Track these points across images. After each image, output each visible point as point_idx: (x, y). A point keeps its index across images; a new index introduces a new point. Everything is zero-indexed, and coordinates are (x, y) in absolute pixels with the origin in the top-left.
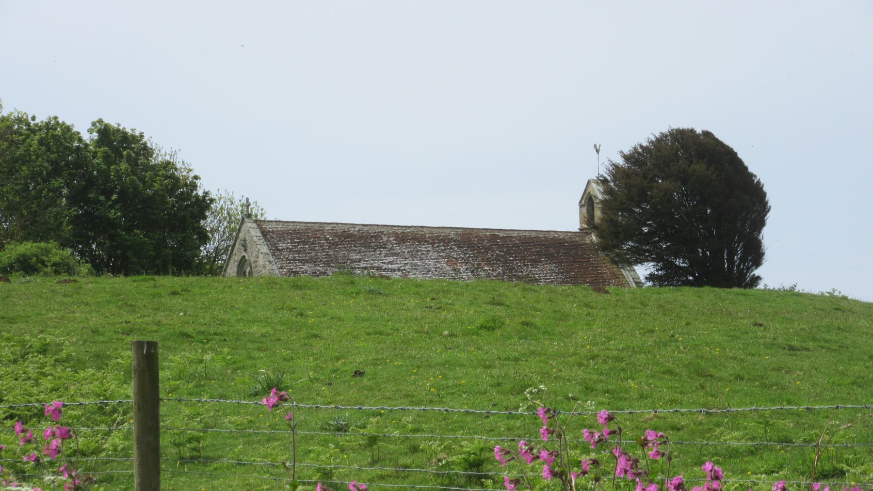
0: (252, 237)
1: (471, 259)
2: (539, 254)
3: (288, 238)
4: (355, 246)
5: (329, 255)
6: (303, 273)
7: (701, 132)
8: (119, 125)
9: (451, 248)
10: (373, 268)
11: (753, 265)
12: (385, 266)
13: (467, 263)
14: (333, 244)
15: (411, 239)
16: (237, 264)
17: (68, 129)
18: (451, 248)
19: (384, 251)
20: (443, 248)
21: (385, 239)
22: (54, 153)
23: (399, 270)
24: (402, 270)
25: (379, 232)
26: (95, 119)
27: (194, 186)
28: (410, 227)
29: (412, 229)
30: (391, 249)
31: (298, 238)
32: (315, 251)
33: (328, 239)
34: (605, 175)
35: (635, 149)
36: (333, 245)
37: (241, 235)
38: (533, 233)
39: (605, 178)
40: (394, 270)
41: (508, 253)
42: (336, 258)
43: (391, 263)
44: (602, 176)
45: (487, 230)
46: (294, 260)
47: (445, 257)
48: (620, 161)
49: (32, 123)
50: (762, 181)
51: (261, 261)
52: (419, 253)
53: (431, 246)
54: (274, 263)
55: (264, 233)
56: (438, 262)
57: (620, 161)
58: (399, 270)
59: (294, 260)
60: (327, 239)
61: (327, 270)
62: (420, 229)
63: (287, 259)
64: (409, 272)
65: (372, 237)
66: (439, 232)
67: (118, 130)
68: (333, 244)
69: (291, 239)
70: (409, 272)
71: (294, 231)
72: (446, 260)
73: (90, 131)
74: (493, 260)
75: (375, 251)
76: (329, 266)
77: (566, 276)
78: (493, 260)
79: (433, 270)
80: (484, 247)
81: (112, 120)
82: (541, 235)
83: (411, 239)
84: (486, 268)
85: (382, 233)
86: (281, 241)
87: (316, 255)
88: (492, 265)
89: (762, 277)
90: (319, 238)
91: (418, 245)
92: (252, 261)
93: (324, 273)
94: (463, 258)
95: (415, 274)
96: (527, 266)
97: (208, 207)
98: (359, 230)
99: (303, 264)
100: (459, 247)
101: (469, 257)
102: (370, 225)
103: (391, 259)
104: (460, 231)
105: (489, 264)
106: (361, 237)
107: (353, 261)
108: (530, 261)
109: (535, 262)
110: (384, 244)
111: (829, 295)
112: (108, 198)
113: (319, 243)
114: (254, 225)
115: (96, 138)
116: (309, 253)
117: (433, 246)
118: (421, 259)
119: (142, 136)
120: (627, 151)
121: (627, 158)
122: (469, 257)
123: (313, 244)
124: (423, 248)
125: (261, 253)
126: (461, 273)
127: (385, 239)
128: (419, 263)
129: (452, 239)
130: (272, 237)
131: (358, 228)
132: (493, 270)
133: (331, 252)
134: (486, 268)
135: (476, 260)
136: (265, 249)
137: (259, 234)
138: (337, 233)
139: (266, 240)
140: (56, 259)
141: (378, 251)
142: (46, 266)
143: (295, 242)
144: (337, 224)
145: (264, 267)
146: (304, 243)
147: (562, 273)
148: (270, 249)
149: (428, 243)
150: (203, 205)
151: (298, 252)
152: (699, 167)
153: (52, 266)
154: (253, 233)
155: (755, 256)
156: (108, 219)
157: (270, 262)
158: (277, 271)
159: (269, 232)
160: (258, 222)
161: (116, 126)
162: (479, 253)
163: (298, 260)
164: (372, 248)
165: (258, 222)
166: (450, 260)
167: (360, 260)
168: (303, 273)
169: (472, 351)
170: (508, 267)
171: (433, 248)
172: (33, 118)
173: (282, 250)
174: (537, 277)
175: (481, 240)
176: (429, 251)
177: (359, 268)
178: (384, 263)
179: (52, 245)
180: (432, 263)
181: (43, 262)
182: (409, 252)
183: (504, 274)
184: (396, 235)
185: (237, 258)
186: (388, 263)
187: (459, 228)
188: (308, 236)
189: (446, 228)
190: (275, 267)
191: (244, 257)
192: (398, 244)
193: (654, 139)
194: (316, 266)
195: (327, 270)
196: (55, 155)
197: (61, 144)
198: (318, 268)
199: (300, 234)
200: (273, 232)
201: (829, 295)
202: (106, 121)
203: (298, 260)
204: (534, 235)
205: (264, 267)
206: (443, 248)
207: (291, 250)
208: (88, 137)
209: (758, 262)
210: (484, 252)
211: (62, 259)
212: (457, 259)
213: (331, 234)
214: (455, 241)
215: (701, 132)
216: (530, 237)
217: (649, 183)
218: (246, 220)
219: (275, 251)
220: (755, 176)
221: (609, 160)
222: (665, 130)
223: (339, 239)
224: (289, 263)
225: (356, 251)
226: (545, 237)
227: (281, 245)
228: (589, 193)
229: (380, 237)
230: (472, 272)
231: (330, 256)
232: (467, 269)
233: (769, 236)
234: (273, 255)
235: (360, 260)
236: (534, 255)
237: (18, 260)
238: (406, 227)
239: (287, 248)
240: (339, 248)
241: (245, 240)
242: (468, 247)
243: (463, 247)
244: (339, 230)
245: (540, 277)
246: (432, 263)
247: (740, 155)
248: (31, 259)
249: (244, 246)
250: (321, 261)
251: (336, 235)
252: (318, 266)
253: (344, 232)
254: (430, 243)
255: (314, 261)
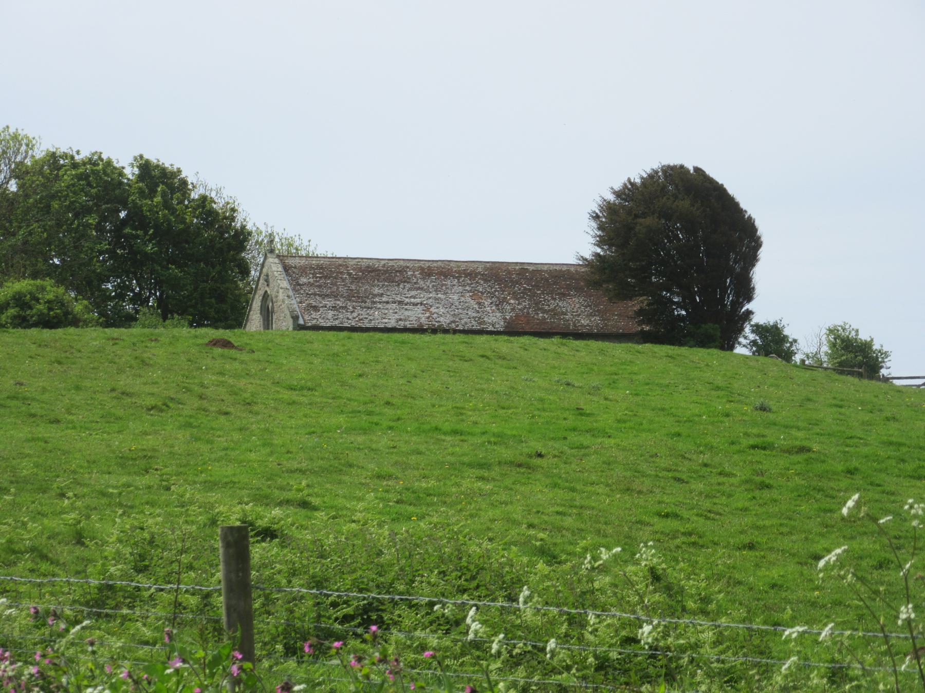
0: (273, 272)
1: (497, 293)
2: (569, 287)
3: (310, 273)
4: (378, 280)
6: (322, 307)
8: (158, 161)
9: (477, 282)
10: (395, 303)
11: (744, 300)
12: (407, 300)
13: (493, 297)
14: (356, 279)
15: (436, 274)
16: (261, 298)
17: (109, 163)
18: (477, 282)
19: (408, 286)
20: (469, 282)
21: (409, 273)
22: (94, 188)
23: (421, 304)
24: (425, 305)
25: (404, 267)
26: (137, 154)
27: (233, 219)
28: (437, 261)
29: (439, 263)
30: (415, 283)
31: (320, 273)
32: (336, 285)
34: (598, 211)
35: (625, 184)
36: (355, 279)
37: (265, 270)
38: (565, 266)
39: (597, 214)
40: (417, 304)
41: (537, 287)
42: (358, 292)
43: (414, 297)
44: (594, 212)
45: (517, 263)
46: (315, 294)
47: (470, 291)
48: (611, 198)
49: (77, 157)
50: (753, 216)
51: (281, 296)
52: (444, 288)
53: (456, 281)
54: (293, 298)
55: (286, 268)
56: (462, 296)
57: (611, 198)
58: (421, 304)
60: (350, 274)
62: (447, 263)
63: (308, 294)
64: (431, 306)
65: (397, 271)
66: (466, 266)
67: (158, 166)
68: (356, 279)
69: (313, 274)
70: (431, 306)
71: (318, 265)
72: (471, 294)
73: (132, 165)
74: (520, 293)
75: (398, 285)
76: (350, 300)
77: (594, 310)
78: (520, 293)
79: (457, 303)
80: (512, 281)
81: (152, 156)
82: (572, 269)
83: (436, 274)
84: (512, 301)
85: (408, 267)
87: (337, 289)
88: (517, 299)
89: (754, 310)
90: (342, 273)
91: (443, 280)
92: (273, 296)
93: (345, 308)
94: (489, 292)
95: (438, 308)
96: (555, 299)
97: (246, 239)
98: (384, 265)
100: (486, 281)
101: (495, 291)
102: (396, 259)
103: (413, 293)
104: (488, 265)
105: (516, 298)
106: (386, 272)
107: (375, 296)
108: (559, 294)
109: (563, 296)
110: (409, 278)
112: (146, 233)
114: (277, 260)
115: (137, 173)
117: (458, 280)
118: (445, 293)
119: (179, 171)
120: (618, 186)
121: (618, 194)
122: (495, 291)
123: (336, 278)
124: (448, 282)
125: (281, 288)
126: (485, 307)
127: (409, 273)
128: (442, 297)
129: (479, 273)
130: (294, 272)
131: (383, 262)
132: (519, 304)
133: (353, 287)
134: (512, 301)
135: (503, 294)
136: (285, 284)
137: (280, 269)
138: (361, 268)
139: (287, 275)
140: (51, 296)
141: (401, 286)
142: (40, 304)
143: (317, 277)
144: (362, 259)
145: (283, 301)
146: (326, 277)
147: (590, 306)
148: (291, 284)
149: (454, 277)
150: (242, 237)
151: (320, 286)
152: (684, 204)
153: (46, 303)
154: (274, 269)
155: (746, 291)
156: (146, 253)
157: (288, 297)
158: (296, 306)
159: (292, 267)
160: (281, 258)
161: (155, 161)
162: (505, 287)
163: (318, 295)
164: (397, 282)
165: (281, 258)
166: (475, 294)
167: (382, 295)
168: (322, 307)
170: (534, 300)
171: (459, 282)
172: (78, 152)
173: (303, 285)
174: (564, 310)
175: (509, 273)
176: (454, 285)
177: (380, 302)
178: (407, 297)
179: (48, 283)
180: (456, 297)
181: (37, 300)
182: (433, 286)
183: (530, 308)
184: (422, 269)
185: (260, 293)
186: (411, 297)
187: (488, 262)
188: (331, 271)
189: (473, 262)
190: (294, 302)
191: (266, 292)
192: (423, 279)
193: (645, 176)
194: (336, 300)
196: (96, 190)
197: (101, 178)
198: (338, 302)
199: (322, 268)
200: (295, 267)
202: (146, 157)
204: (565, 268)
205: (283, 301)
206: (469, 282)
208: (131, 172)
209: (749, 299)
210: (511, 286)
211: (57, 297)
212: (482, 293)
214: (482, 275)
216: (561, 271)
217: (633, 219)
218: (269, 255)
219: (296, 286)
220: (746, 211)
221: (601, 196)
222: (656, 166)
223: (363, 273)
225: (378, 285)
226: (576, 271)
227: (303, 280)
229: (405, 271)
230: (497, 305)
231: (352, 290)
232: (491, 303)
233: (760, 275)
234: (294, 290)
235: (382, 295)
236: (563, 288)
237: (14, 298)
238: (433, 261)
239: (309, 282)
240: (362, 283)
241: (267, 275)
242: (495, 281)
243: (489, 281)
244: (364, 264)
245: (567, 310)
246: (456, 297)
247: (731, 191)
248: (25, 296)
249: (267, 281)
250: (342, 295)
251: (360, 270)
252: (339, 300)
253: (368, 267)
254: (456, 277)
255: (335, 296)
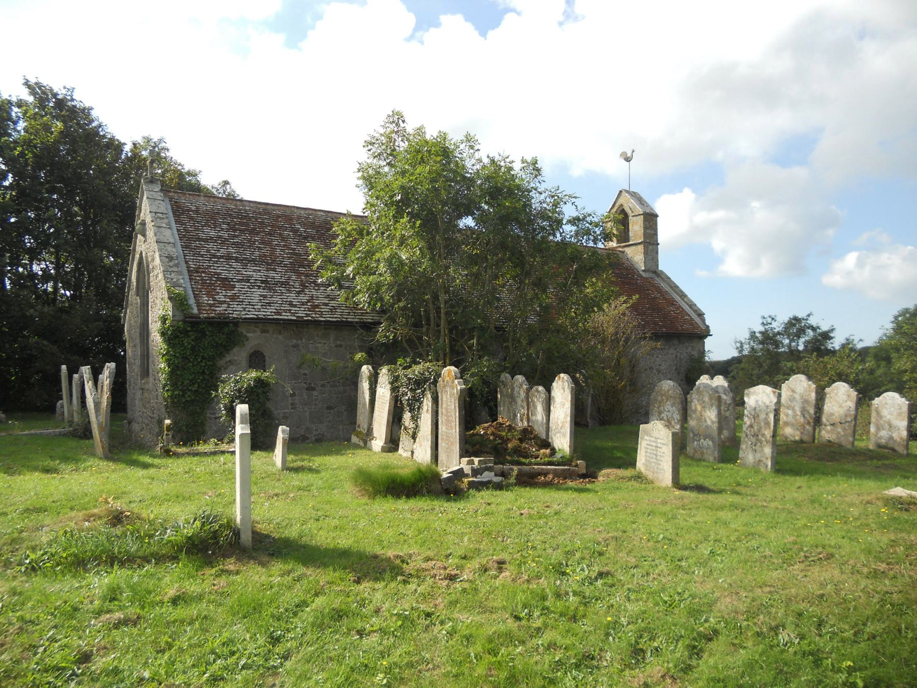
5: (296, 254)
7: (444, 19)
31: (241, 224)
33: (298, 230)
59: (228, 257)
60: (296, 231)
61: (289, 278)
86: (209, 226)
99: (245, 266)
111: (135, 457)
113: (280, 234)
116: (260, 248)
123: (270, 234)
169: (559, 482)
195: (289, 278)
201: (135, 457)
203: (237, 259)
207: (224, 242)
213: (303, 224)
215: (444, 19)
223: (317, 231)
224: (216, 262)
228: (622, 205)
255: (270, 263)
